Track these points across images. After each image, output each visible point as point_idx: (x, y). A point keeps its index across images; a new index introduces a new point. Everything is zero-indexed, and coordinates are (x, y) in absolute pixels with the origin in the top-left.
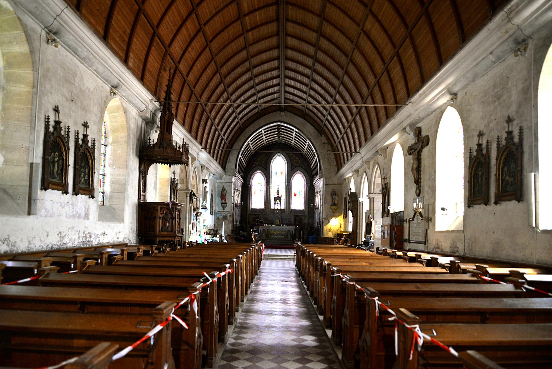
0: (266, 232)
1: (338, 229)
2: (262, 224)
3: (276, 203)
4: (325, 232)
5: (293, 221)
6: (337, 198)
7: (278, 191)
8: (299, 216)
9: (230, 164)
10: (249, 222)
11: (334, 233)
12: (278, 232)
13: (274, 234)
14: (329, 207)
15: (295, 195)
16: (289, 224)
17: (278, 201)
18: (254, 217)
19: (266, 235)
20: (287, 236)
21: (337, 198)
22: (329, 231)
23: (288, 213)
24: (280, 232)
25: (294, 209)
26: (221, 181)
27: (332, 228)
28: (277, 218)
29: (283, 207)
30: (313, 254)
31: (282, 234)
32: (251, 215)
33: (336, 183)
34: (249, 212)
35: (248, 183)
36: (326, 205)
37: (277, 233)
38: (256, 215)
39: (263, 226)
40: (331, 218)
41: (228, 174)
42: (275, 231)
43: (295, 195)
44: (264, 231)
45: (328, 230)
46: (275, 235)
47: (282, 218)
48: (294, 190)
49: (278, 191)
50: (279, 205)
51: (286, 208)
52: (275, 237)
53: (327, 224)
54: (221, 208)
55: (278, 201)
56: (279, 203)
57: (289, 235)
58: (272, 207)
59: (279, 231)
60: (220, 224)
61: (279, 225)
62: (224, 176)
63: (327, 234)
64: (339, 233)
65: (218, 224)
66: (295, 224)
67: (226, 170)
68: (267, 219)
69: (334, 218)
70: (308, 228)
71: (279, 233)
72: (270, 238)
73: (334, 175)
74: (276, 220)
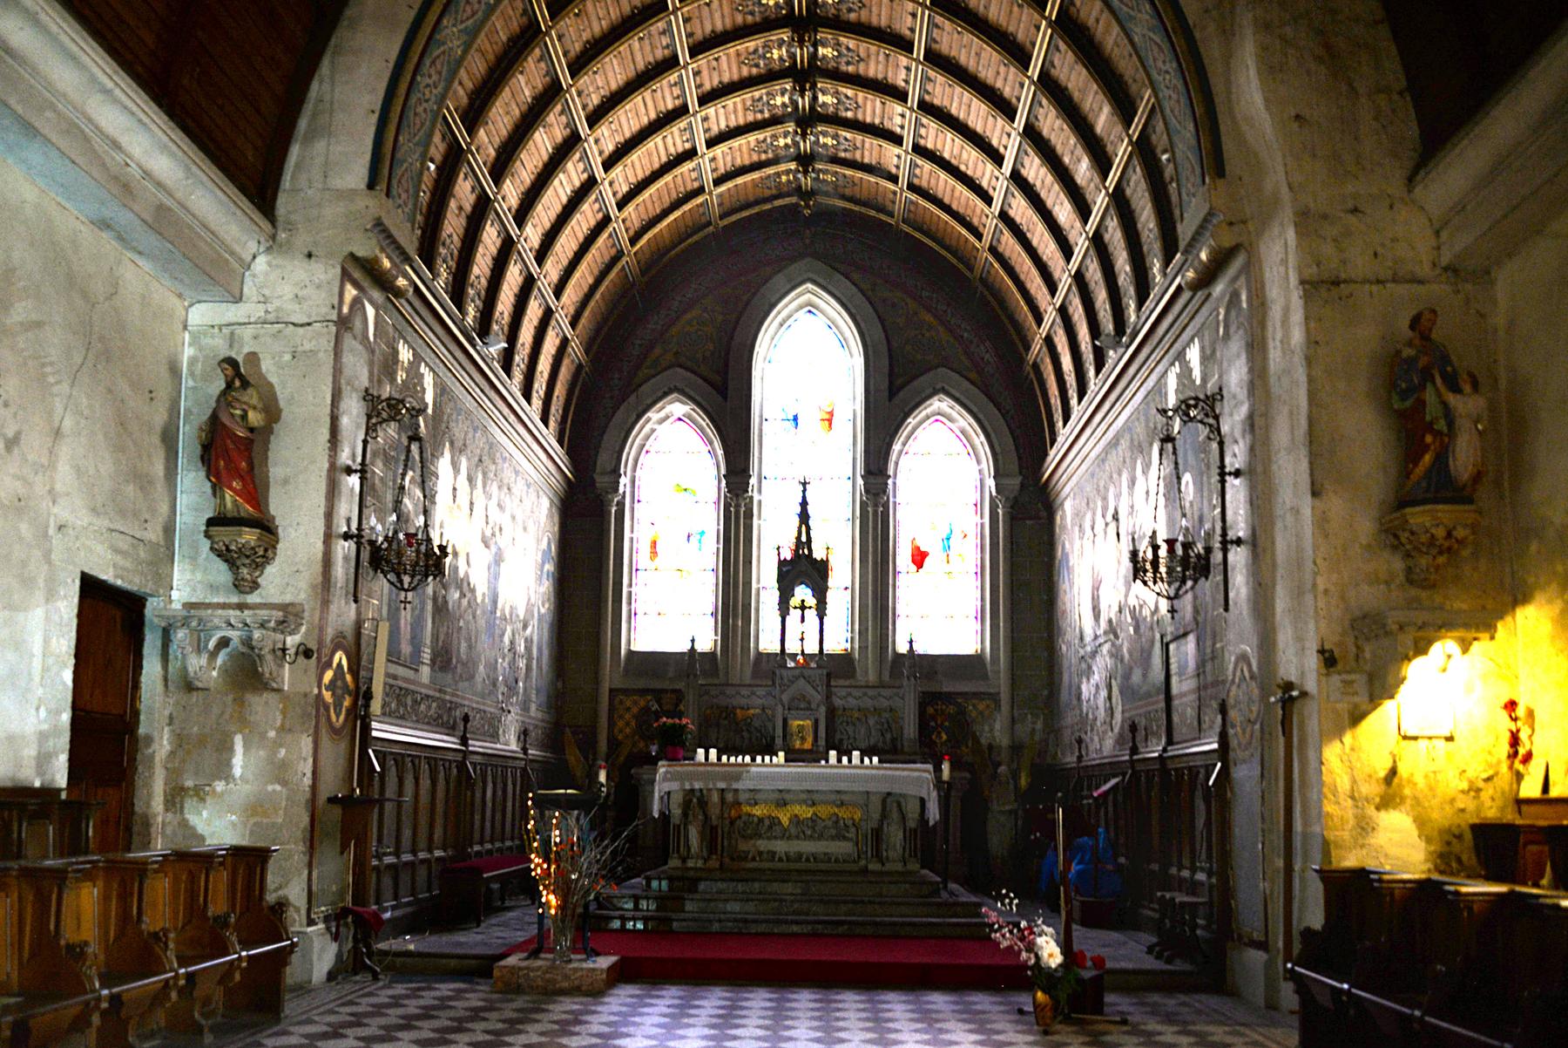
0: (714, 812)
1: (1478, 771)
2: (676, 746)
3: (795, 601)
4: (1337, 811)
5: (910, 729)
6: (1466, 405)
7: (804, 517)
8: (949, 697)
9: (320, 146)
10: (613, 744)
11: (1440, 816)
12: (806, 812)
13: (775, 822)
14: (1366, 527)
15: (919, 558)
16: (890, 752)
17: (803, 593)
18: (646, 710)
19: (711, 836)
20: (877, 834)
21: (1466, 405)
22: (1387, 801)
23: (872, 677)
24: (824, 811)
25: (929, 645)
26: (233, 313)
27: (1416, 766)
28: (800, 705)
29: (839, 638)
30: (753, 760)
31: (839, 830)
32: (626, 692)
33: (1425, 270)
34: (610, 678)
35: (601, 481)
36: (1336, 504)
37: (796, 820)
38: (658, 694)
39: (683, 768)
40: (1421, 649)
41: (302, 240)
42: (782, 804)
43: (919, 558)
44: (694, 801)
45: (1371, 790)
46: (785, 835)
47: (832, 713)
48: (908, 529)
49: (804, 517)
50: (811, 615)
51: (863, 648)
52: (780, 847)
53: (1356, 718)
54: (220, 572)
55: (803, 593)
56: (811, 601)
57: (895, 836)
58: (768, 642)
59: (811, 798)
60: (202, 741)
61: (815, 756)
62: (261, 263)
63: (1364, 827)
64: (1491, 812)
65: (180, 740)
66: (927, 751)
67: (283, 204)
68: (728, 712)
69: (1444, 647)
70: (1015, 775)
71: (814, 820)
72: (744, 857)
73: (1396, 187)
74: (795, 724)
